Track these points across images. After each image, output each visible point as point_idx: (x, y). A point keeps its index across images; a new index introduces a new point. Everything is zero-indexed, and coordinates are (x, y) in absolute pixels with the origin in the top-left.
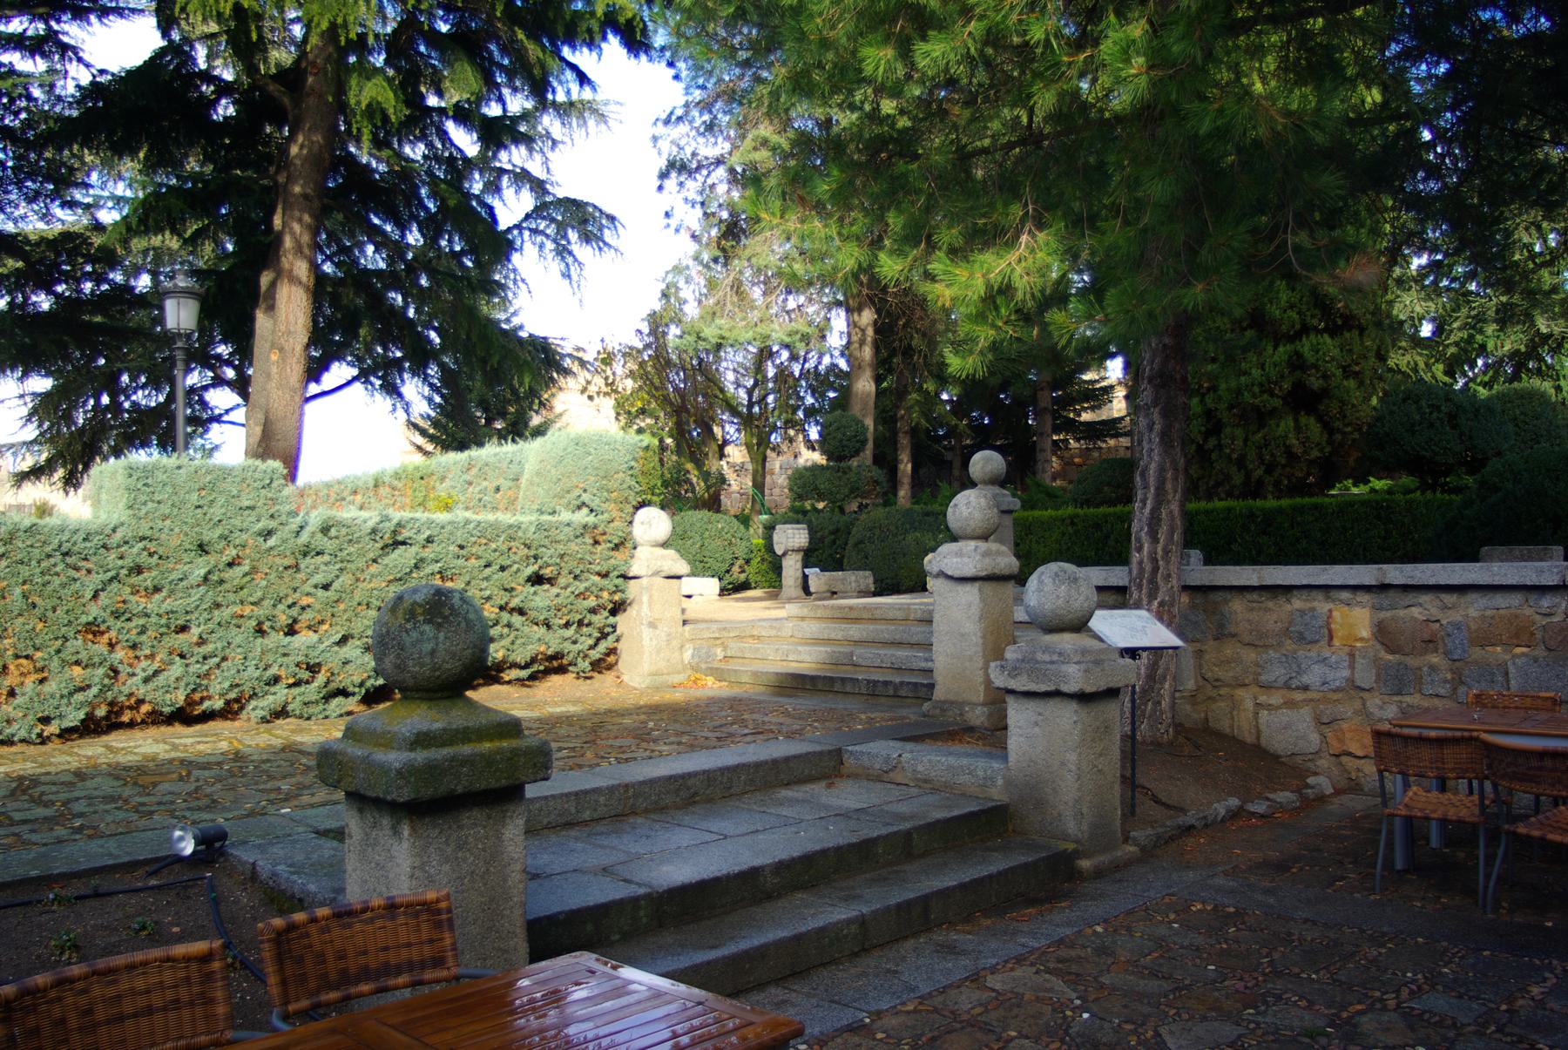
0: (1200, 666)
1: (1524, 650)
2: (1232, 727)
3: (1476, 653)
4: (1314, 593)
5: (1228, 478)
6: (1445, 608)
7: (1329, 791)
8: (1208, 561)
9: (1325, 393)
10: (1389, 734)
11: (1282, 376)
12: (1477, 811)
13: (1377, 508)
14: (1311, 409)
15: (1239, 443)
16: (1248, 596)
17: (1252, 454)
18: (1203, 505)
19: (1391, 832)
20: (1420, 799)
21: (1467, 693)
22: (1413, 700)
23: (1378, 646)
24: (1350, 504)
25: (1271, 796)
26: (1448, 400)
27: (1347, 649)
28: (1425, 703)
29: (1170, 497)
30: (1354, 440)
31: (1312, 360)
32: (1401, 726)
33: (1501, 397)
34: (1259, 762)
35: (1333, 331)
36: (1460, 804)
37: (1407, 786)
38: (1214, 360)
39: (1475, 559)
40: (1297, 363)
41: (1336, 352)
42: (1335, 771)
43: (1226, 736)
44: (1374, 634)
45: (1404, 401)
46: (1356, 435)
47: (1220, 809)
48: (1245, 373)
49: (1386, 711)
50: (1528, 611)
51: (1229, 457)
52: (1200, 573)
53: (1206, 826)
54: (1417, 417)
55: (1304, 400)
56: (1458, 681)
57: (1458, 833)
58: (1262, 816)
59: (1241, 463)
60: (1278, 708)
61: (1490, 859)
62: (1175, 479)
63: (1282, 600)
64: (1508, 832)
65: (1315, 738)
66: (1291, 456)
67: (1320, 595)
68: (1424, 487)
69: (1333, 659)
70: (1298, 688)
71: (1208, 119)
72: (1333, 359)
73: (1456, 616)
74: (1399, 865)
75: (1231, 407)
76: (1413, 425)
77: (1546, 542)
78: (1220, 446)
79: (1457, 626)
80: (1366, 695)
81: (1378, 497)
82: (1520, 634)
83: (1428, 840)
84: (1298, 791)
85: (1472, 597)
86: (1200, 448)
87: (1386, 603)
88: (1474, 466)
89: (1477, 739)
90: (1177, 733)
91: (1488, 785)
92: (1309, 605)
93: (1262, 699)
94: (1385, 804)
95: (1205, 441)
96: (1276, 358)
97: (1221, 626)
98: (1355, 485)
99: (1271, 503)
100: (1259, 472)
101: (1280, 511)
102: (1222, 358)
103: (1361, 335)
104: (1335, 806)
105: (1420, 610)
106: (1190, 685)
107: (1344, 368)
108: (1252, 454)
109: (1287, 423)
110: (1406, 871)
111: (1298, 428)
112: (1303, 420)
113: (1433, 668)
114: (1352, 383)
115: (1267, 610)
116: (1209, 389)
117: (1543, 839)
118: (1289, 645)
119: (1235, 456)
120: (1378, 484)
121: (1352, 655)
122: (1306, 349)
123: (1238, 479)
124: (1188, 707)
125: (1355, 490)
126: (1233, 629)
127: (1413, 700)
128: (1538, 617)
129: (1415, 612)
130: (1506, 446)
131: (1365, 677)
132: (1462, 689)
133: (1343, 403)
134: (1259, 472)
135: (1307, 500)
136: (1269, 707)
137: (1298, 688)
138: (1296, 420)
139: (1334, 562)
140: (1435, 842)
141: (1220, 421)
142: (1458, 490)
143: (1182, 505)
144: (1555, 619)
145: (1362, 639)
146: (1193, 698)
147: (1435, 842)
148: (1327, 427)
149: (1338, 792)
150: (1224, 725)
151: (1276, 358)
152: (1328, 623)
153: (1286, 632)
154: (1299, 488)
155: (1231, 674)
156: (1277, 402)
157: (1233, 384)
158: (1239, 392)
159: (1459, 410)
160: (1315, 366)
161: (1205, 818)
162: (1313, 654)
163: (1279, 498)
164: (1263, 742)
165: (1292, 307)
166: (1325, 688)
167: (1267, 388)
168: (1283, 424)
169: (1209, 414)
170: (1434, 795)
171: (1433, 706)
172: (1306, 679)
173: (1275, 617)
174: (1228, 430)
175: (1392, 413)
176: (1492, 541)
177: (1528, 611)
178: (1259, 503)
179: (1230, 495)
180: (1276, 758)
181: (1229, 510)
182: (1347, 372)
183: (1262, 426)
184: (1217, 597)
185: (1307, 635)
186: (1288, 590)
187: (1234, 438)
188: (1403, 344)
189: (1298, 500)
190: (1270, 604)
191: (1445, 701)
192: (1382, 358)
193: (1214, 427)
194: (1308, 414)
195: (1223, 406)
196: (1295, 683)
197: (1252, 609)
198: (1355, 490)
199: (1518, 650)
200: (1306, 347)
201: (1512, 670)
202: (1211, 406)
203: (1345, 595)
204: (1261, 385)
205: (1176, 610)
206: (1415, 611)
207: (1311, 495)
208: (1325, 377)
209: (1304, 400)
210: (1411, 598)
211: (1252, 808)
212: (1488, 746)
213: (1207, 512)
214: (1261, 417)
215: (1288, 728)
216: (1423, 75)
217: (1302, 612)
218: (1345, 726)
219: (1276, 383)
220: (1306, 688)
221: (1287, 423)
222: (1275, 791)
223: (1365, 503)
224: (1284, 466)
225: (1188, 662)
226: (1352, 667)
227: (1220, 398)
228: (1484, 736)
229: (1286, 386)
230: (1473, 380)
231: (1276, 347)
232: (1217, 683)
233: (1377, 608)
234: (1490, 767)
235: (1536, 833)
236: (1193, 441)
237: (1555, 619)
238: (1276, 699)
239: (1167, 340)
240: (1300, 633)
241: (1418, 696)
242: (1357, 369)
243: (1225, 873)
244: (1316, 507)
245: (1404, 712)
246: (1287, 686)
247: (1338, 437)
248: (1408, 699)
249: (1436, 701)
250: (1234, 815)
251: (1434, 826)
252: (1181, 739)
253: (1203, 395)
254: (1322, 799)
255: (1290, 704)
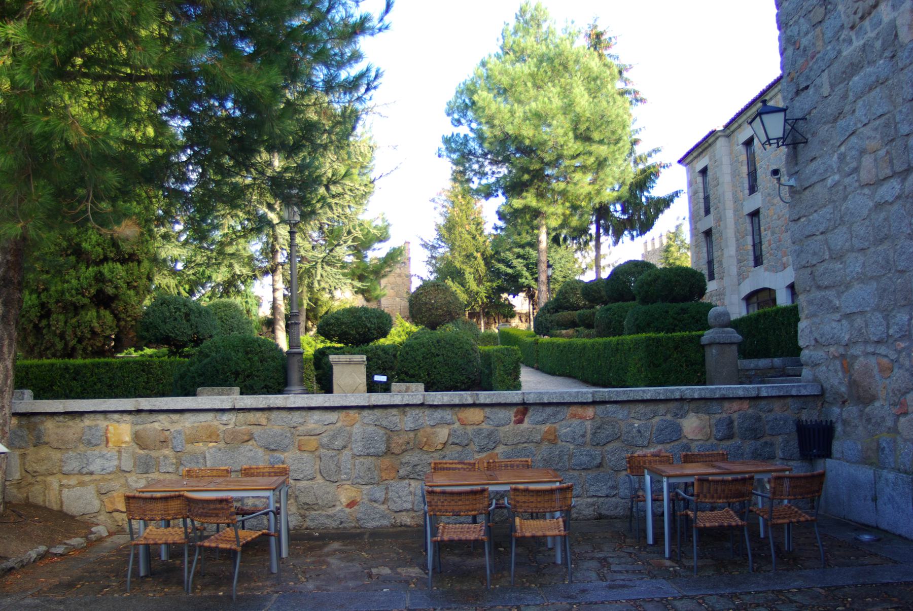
0: (24, 464)
1: (214, 444)
2: (44, 501)
3: (189, 447)
4: (98, 416)
5: (53, 345)
6: (173, 422)
7: (105, 534)
8: (37, 397)
9: (115, 297)
10: (134, 497)
11: (91, 286)
12: (183, 536)
13: (144, 366)
14: (107, 306)
15: (61, 324)
16: (57, 418)
17: (69, 331)
18: (35, 361)
19: (136, 556)
20: (155, 533)
21: (183, 470)
22: (154, 476)
23: (135, 446)
24: (126, 363)
25: (67, 542)
26: (185, 305)
27: (117, 449)
28: (161, 477)
29: (6, 356)
30: (132, 326)
31: (109, 277)
32: (143, 492)
33: (215, 306)
34: (63, 521)
35: (123, 261)
36: (175, 534)
37: (146, 526)
38: (48, 272)
39: (195, 395)
40: (99, 278)
41: (123, 274)
42: (109, 521)
43: (41, 507)
44: (133, 439)
45: (162, 304)
46: (133, 323)
47: (33, 554)
48: (67, 282)
49: (137, 483)
50: (216, 423)
51: (55, 332)
52: (27, 402)
53: (23, 566)
54: (168, 314)
55: (103, 300)
56: (180, 463)
57: (175, 551)
58: (61, 555)
59: (62, 336)
60: (74, 487)
61: (190, 562)
62: (10, 345)
63: (78, 420)
64: (200, 547)
65: (97, 504)
66: (94, 333)
67: (100, 417)
68: (171, 353)
69: (109, 455)
70: (87, 474)
71: (39, 126)
72: (122, 278)
73: (178, 427)
74: (142, 574)
75: (57, 302)
76: (165, 318)
77: (231, 385)
78: (49, 326)
79: (179, 432)
80: (127, 475)
81: (144, 359)
82: (212, 436)
83: (160, 556)
84: (86, 537)
85: (188, 415)
86: (36, 327)
87: (140, 420)
88: (197, 342)
89: (182, 496)
90: (5, 508)
91: (188, 520)
92: (95, 423)
93: (64, 482)
94: (132, 539)
95: (39, 321)
96: (87, 274)
97: (39, 438)
98: (135, 351)
99: (79, 361)
100: (74, 342)
101: (85, 366)
102: (52, 271)
103: (139, 265)
104: (108, 543)
105: (160, 423)
106: (17, 476)
107: (128, 283)
108: (69, 331)
109: (91, 314)
110: (146, 576)
111: (99, 317)
112: (103, 312)
113: (165, 457)
114: (132, 292)
115: (68, 427)
116: (44, 290)
117: (217, 547)
118: (82, 447)
119: (58, 332)
120: (148, 351)
121: (119, 452)
122: (106, 270)
123: (60, 346)
124: (15, 491)
125: (134, 355)
126: (46, 439)
127: (154, 476)
128: (221, 426)
129: (156, 425)
130: (215, 332)
131: (127, 464)
132: (181, 468)
133: (126, 303)
134: (74, 342)
135: (102, 360)
136: (69, 487)
137: (87, 474)
138: (98, 312)
139: (116, 397)
140: (164, 557)
141: (50, 310)
142: (187, 356)
143: (14, 361)
144: (230, 427)
145: (125, 442)
146: (18, 485)
147: (164, 557)
148: (116, 316)
149: (111, 534)
150: (40, 500)
151: (87, 274)
152: (106, 433)
153: (80, 440)
154: (100, 353)
155: (45, 467)
156: (86, 301)
157: (59, 288)
158: (63, 293)
159: (191, 313)
160: (111, 281)
161: (22, 561)
162: (96, 452)
163: (85, 358)
164: (65, 509)
165: (99, 245)
166: (103, 472)
167: (80, 292)
168: (89, 314)
169: (43, 305)
170: (162, 529)
171: (165, 479)
172: (92, 468)
173: (73, 431)
174: (54, 316)
175: (154, 311)
176: (203, 385)
177: (216, 423)
178: (72, 361)
179: (54, 355)
180: (72, 517)
181: (53, 365)
182: (129, 285)
183: (76, 314)
184: (33, 419)
185: (93, 441)
186: (81, 414)
187: (58, 320)
188: (165, 272)
189: (97, 360)
190: (71, 423)
191: (172, 475)
192: (150, 279)
193: (45, 312)
194: (105, 308)
195: (52, 301)
196: (85, 471)
197: (59, 427)
198: (134, 355)
199: (211, 444)
200: (106, 269)
201: (207, 455)
202: (45, 300)
203: (116, 416)
204: (77, 289)
205: (7, 429)
206: (156, 425)
207: (105, 357)
208: (116, 287)
209: (103, 300)
210: (154, 417)
211: (54, 550)
212: (190, 501)
213: (38, 366)
214: (76, 309)
215: (79, 498)
216: (179, 125)
217: (90, 427)
218: (115, 494)
219: (86, 289)
220: (92, 473)
221: (91, 314)
222: (71, 538)
223: (136, 362)
224: (89, 339)
225: (15, 461)
226: (119, 459)
227: (50, 296)
228: (186, 494)
229: (93, 291)
230: (203, 297)
231: (87, 268)
232: (35, 474)
233: (135, 424)
234: (189, 511)
235: (214, 545)
236: (31, 321)
237: (230, 427)
238: (73, 481)
239: (9, 258)
240: (89, 440)
241: (157, 473)
242: (136, 284)
243: (33, 595)
244: (107, 364)
245: (149, 484)
246: (80, 473)
247: (122, 323)
248: (151, 476)
249: (167, 476)
250: (42, 557)
251: (163, 547)
252: (8, 512)
253: (40, 293)
254: (100, 539)
255: (82, 484)
